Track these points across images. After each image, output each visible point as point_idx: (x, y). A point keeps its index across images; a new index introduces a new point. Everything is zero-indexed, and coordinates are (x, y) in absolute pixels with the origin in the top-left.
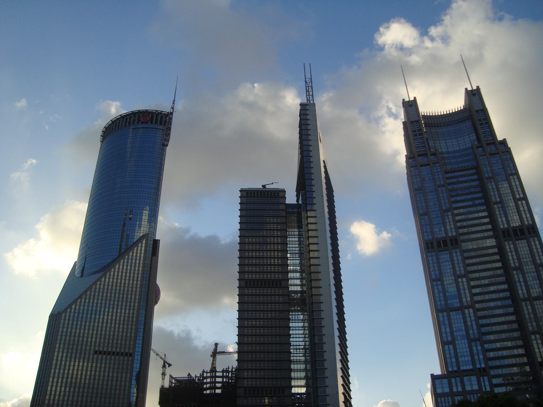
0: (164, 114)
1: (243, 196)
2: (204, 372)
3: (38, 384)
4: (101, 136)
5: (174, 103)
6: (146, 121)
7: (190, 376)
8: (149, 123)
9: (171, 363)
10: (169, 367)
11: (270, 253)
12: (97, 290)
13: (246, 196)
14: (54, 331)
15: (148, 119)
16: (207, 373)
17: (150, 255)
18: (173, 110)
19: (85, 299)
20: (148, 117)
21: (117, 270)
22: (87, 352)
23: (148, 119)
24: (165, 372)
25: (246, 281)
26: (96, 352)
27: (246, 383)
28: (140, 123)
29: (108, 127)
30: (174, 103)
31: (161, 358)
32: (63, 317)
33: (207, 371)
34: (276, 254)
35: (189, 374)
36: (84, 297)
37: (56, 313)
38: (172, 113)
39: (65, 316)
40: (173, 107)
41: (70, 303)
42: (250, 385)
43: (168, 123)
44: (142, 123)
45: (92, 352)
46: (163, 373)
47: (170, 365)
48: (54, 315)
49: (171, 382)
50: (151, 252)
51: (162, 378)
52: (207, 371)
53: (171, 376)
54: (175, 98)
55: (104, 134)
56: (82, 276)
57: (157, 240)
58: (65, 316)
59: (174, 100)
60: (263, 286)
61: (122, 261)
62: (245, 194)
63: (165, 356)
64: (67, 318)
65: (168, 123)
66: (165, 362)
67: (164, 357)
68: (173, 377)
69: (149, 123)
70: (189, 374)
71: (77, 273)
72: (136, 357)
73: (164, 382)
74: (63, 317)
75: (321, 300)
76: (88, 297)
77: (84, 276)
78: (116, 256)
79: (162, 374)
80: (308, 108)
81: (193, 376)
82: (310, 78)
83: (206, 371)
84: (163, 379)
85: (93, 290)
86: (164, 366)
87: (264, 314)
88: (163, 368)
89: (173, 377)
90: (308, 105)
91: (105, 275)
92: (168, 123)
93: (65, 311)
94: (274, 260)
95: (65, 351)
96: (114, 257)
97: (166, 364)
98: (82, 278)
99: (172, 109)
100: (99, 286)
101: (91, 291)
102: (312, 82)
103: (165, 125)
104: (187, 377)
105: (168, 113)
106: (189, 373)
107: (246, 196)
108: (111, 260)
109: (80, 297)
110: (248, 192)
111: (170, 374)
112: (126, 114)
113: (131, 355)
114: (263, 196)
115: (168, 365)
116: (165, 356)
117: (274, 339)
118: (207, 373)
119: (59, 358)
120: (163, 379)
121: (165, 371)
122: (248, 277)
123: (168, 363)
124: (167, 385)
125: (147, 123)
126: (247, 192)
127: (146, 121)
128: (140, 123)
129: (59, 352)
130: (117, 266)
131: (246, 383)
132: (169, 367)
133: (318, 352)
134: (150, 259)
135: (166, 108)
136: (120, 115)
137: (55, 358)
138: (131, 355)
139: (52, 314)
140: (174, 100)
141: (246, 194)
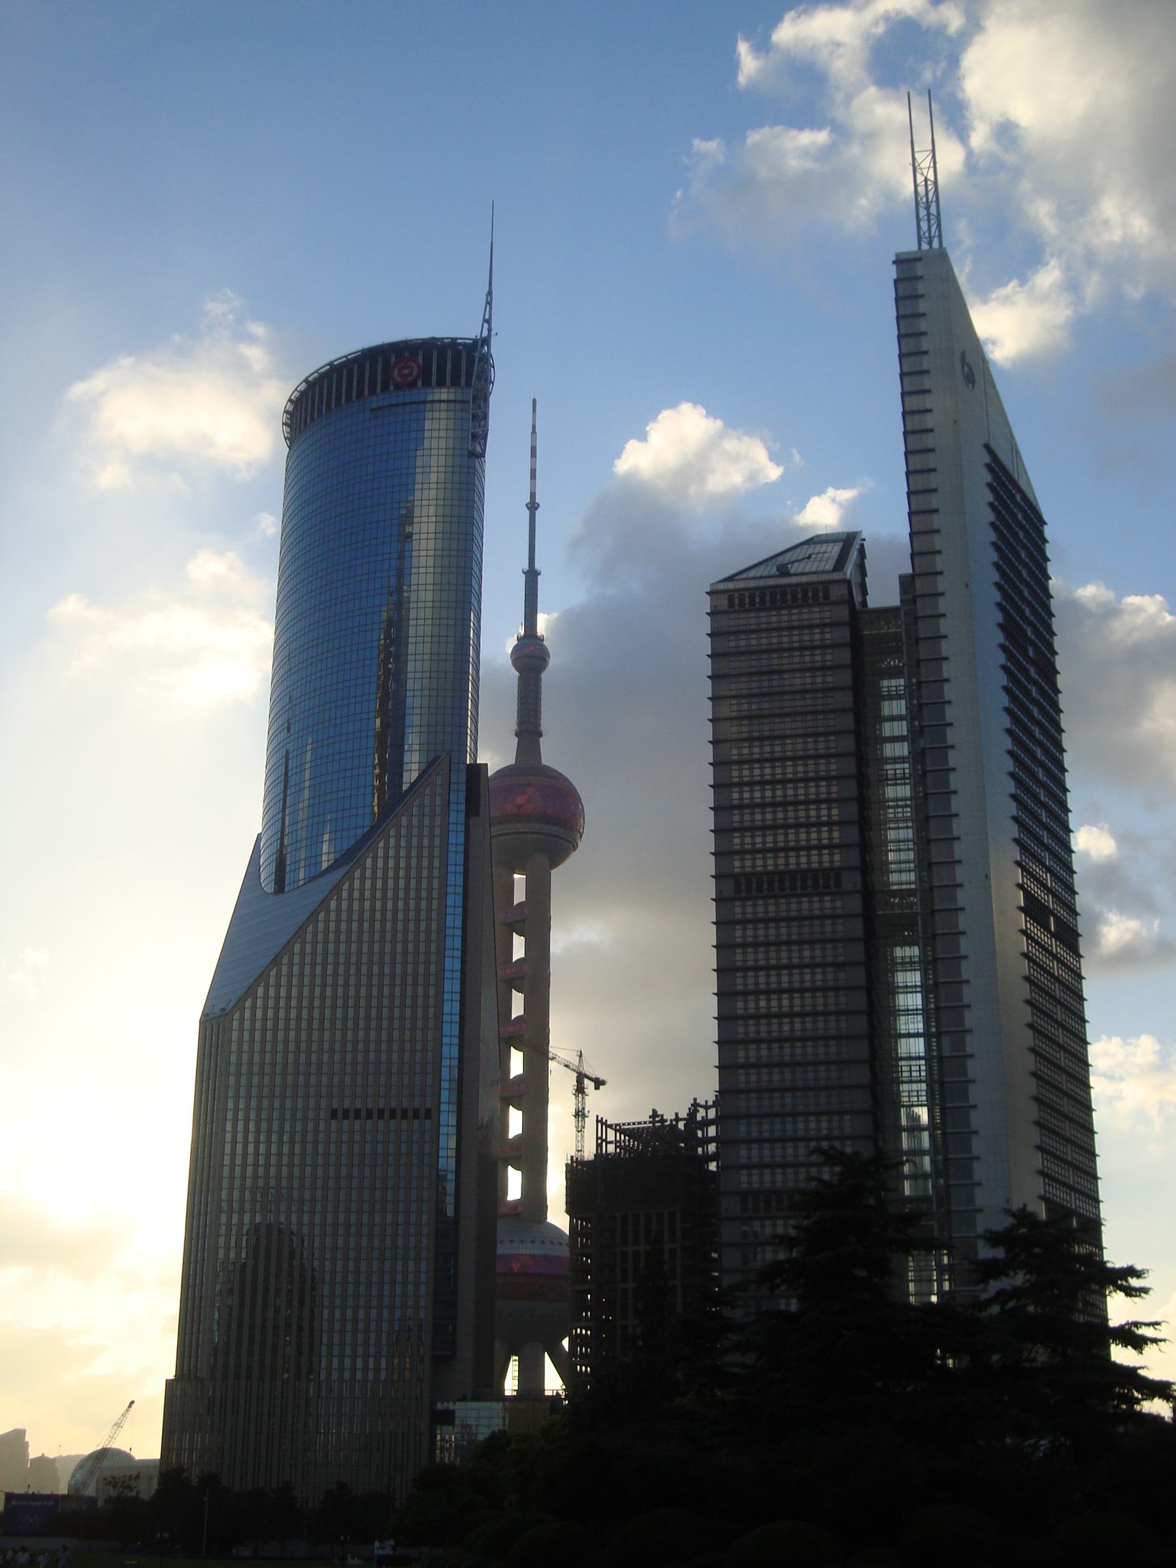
0: (465, 345)
1: (719, 608)
2: (695, 1105)
3: (193, 1216)
4: (283, 424)
5: (489, 303)
6: (410, 379)
7: (657, 1119)
8: (419, 383)
9: (602, 1077)
10: (597, 1088)
11: (807, 788)
12: (320, 937)
13: (726, 608)
14: (217, 1063)
15: (415, 372)
16: (706, 1107)
17: (462, 818)
18: (490, 330)
19: (291, 965)
20: (413, 364)
21: (368, 874)
22: (398, 981)
23: (415, 372)
24: (583, 1109)
25: (736, 877)
26: (334, 1114)
27: (744, 1179)
28: (392, 388)
29: (299, 399)
30: (489, 303)
31: (566, 1066)
32: (235, 1024)
33: (706, 1102)
34: (823, 790)
35: (655, 1114)
36: (285, 960)
37: (217, 1010)
38: (486, 341)
39: (242, 1019)
40: (487, 317)
41: (251, 981)
42: (767, 1185)
43: (479, 378)
44: (398, 387)
45: (322, 1114)
46: (579, 1111)
47: (598, 1083)
48: (211, 1016)
49: (601, 1141)
50: (463, 807)
51: (577, 1127)
52: (706, 1102)
53: (599, 1121)
54: (490, 284)
55: (291, 419)
56: (280, 885)
57: (480, 765)
58: (242, 1019)
59: (490, 293)
60: (788, 891)
61: (381, 844)
62: (723, 603)
63: (581, 1056)
64: (247, 1024)
65: (477, 377)
66: (581, 1077)
67: (577, 1063)
68: (608, 1123)
69: (419, 383)
70: (655, 1114)
71: (266, 874)
72: (443, 1118)
73: (582, 1136)
74: (235, 1024)
75: (969, 1074)
76: (296, 959)
77: (286, 889)
78: (366, 830)
79: (574, 1114)
80: (920, 269)
81: (669, 1116)
82: (931, 148)
83: (703, 1103)
84: (581, 1131)
85: (309, 937)
86: (580, 1090)
87: (824, 949)
88: (577, 1096)
89: (608, 1123)
90: (919, 259)
91: (349, 876)
92: (479, 378)
93: (239, 1005)
94: (818, 809)
95: (252, 1116)
96: (360, 832)
97: (586, 1081)
98: (281, 897)
99: (486, 325)
100: (274, 1034)
101: (304, 943)
102: (935, 163)
103: (468, 384)
104: (650, 1122)
105: (475, 341)
106: (654, 1111)
107: (726, 608)
108: (352, 842)
109: (276, 962)
110: (733, 595)
111: (597, 1117)
112: (345, 359)
113: (428, 1114)
114: (779, 603)
115: (592, 1084)
116: (581, 1056)
117: (822, 1050)
118: (706, 1107)
119: (240, 1137)
120: (580, 1130)
121: (583, 1103)
122: (743, 867)
123: (594, 1077)
124: (589, 1153)
125: (413, 385)
126: (729, 596)
127: (410, 379)
128: (392, 388)
129: (235, 1120)
130: (369, 862)
131: (744, 1179)
132: (597, 1088)
133: (952, 1082)
134: (462, 828)
135: (466, 329)
136: (328, 364)
137: (228, 1138)
138: (428, 1114)
139: (208, 1015)
140: (490, 293)
141: (727, 602)
